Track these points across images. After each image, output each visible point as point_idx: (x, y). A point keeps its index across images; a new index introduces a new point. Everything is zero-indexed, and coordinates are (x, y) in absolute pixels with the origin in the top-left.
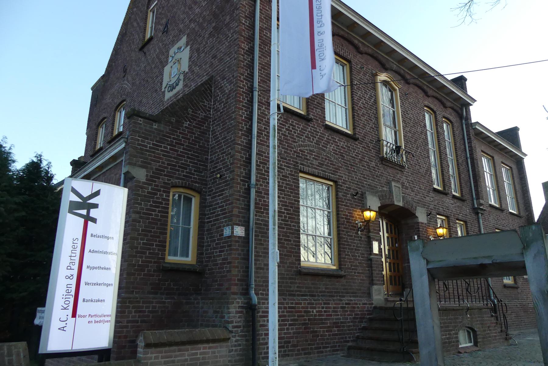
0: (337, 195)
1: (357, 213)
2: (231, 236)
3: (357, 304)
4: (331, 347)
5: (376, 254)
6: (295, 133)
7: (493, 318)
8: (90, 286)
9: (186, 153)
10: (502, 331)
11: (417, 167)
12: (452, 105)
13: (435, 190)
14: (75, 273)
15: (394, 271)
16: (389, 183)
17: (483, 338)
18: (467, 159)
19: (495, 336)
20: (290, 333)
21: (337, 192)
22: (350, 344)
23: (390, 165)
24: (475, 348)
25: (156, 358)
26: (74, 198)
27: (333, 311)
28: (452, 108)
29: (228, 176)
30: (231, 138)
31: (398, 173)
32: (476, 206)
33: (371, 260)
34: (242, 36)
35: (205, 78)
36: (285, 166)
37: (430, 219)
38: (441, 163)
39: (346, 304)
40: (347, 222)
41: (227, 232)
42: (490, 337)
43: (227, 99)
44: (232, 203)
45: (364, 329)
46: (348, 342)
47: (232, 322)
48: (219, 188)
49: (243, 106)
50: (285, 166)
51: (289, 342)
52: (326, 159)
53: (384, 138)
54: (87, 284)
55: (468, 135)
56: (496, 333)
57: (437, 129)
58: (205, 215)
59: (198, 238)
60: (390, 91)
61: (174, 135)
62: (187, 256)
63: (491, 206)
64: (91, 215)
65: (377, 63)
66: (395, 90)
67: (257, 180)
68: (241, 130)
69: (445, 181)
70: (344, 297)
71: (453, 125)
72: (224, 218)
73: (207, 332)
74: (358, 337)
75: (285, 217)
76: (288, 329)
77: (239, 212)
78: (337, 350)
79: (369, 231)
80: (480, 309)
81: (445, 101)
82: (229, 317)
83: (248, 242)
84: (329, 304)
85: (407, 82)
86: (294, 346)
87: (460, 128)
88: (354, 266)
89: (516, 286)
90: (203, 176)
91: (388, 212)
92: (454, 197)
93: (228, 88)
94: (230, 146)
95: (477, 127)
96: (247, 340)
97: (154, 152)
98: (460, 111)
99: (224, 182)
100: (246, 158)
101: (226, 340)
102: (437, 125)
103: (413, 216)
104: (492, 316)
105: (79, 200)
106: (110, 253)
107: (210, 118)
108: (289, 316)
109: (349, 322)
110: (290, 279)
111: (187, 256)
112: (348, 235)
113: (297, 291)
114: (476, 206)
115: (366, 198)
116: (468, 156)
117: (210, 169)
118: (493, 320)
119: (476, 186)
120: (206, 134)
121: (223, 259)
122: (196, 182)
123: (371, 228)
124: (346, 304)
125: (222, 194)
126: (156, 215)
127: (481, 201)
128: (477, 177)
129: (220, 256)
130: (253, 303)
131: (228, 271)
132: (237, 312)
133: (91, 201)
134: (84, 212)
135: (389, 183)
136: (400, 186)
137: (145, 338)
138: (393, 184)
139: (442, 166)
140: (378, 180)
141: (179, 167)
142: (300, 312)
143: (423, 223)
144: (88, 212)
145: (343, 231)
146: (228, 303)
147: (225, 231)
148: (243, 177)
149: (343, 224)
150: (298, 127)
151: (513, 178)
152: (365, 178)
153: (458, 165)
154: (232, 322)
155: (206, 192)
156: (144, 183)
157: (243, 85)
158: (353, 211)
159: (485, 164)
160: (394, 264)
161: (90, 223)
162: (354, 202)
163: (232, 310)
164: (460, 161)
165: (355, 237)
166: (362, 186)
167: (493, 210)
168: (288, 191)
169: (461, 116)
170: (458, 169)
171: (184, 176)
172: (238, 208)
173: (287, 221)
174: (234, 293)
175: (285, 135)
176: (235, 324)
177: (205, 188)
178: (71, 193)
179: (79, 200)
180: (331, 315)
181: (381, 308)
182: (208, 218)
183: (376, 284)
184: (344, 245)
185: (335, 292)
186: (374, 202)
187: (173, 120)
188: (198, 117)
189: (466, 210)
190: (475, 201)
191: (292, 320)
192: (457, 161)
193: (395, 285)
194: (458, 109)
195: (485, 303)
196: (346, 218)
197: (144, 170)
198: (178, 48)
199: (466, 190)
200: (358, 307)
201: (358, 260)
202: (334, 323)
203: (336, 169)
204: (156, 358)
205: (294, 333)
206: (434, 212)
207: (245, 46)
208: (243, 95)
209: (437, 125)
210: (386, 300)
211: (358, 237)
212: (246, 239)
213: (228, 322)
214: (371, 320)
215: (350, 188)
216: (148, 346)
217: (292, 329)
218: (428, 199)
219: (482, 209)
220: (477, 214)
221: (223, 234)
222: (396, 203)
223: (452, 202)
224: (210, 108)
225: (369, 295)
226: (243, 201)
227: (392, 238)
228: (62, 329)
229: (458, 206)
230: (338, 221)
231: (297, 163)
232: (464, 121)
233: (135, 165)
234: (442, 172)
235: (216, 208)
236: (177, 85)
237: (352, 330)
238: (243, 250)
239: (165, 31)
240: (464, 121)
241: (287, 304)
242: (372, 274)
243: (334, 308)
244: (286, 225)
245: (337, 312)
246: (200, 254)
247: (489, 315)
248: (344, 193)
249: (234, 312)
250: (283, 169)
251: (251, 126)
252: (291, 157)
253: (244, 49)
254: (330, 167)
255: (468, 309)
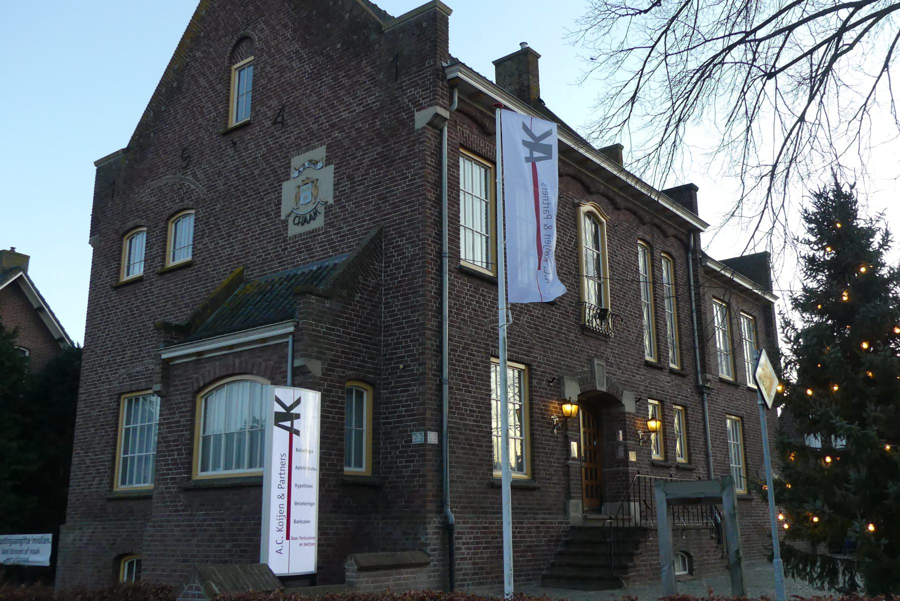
0: (530, 382)
1: (553, 405)
2: (425, 444)
3: (552, 523)
4: (525, 575)
5: (574, 459)
6: (485, 305)
7: (712, 541)
8: (299, 506)
9: (360, 336)
10: (722, 558)
11: (626, 333)
12: (675, 232)
13: (647, 364)
14: (285, 492)
15: (591, 478)
16: (590, 361)
17: (700, 565)
18: (692, 312)
19: (714, 564)
20: (483, 558)
21: (530, 378)
22: (544, 572)
23: (593, 335)
24: (690, 577)
25: (367, 582)
26: (278, 408)
27: (527, 532)
28: (675, 237)
29: (415, 367)
30: (418, 320)
31: (601, 345)
32: (701, 383)
33: (568, 466)
34: (428, 182)
35: (373, 233)
36: (476, 351)
37: (639, 406)
38: (656, 322)
39: (542, 523)
40: (543, 418)
41: (417, 438)
42: (708, 564)
43: (409, 266)
44: (424, 403)
45: (560, 554)
46: (542, 569)
47: (430, 544)
48: (401, 382)
49: (432, 278)
50: (476, 351)
51: (483, 568)
52: (519, 336)
53: (587, 300)
54: (296, 504)
55: (696, 276)
56: (715, 559)
57: (653, 272)
58: (380, 413)
59: (373, 444)
60: (594, 223)
61: (346, 313)
62: (361, 466)
63: (722, 380)
64: (295, 427)
65: (579, 186)
66: (601, 223)
67: (450, 374)
68: (431, 311)
69: (660, 352)
70: (537, 514)
71: (674, 262)
72: (412, 421)
73: (408, 556)
74: (553, 564)
75: (477, 416)
76: (482, 553)
77: (432, 415)
78: (531, 580)
79: (567, 429)
80: (698, 529)
81: (664, 226)
82: (427, 539)
83: (442, 451)
84: (522, 523)
85: (616, 207)
86: (487, 573)
87: (685, 266)
88: (549, 475)
89: (749, 497)
90: (377, 364)
91: (588, 401)
92: (672, 371)
93: (409, 252)
94: (417, 330)
95: (708, 264)
96: (443, 565)
97: (327, 339)
98: (685, 241)
99: (409, 376)
100: (437, 346)
101: (426, 564)
102: (653, 266)
103: (619, 403)
104: (712, 538)
105: (283, 411)
106: (305, 468)
107: (381, 285)
108: (483, 538)
109: (543, 546)
110: (482, 493)
111: (361, 466)
112: (543, 436)
113: (489, 508)
114: (701, 383)
115: (564, 385)
116: (694, 307)
117: (385, 355)
118: (714, 543)
119: (703, 353)
120: (378, 307)
121: (412, 471)
122: (370, 373)
123: (569, 424)
124: (542, 523)
125: (408, 391)
126: (333, 418)
127: (709, 376)
128: (705, 337)
129: (409, 467)
130: (450, 522)
131: (420, 486)
132: (434, 533)
133: (294, 411)
134: (288, 424)
135: (589, 360)
136: (604, 364)
137: (356, 561)
138: (596, 361)
139: (657, 328)
140: (578, 357)
141: (353, 354)
142: (494, 533)
143: (630, 414)
144: (292, 424)
145: (537, 430)
146: (425, 523)
147: (414, 437)
148: (435, 370)
149: (538, 421)
150: (489, 297)
151: (757, 334)
152: (562, 356)
153: (679, 322)
154: (430, 544)
155: (380, 384)
156: (321, 379)
157: (431, 249)
158: (549, 402)
159: (717, 315)
160: (591, 469)
161: (294, 436)
162: (550, 390)
163: (430, 531)
164: (682, 317)
165: (550, 437)
166: (559, 368)
167: (725, 387)
168: (479, 384)
169: (686, 247)
170: (679, 328)
171: (358, 365)
172: (431, 409)
173: (478, 422)
174: (430, 512)
175: (475, 310)
176: (433, 547)
177: (379, 379)
178: (276, 403)
179: (283, 411)
180: (525, 537)
181: (579, 528)
182: (384, 419)
183: (573, 498)
184: (538, 448)
185: (529, 509)
186: (572, 389)
187: (345, 293)
188: (369, 286)
189: (687, 388)
190: (700, 375)
191: (486, 542)
192: (678, 316)
193: (592, 497)
194: (683, 237)
195: (705, 521)
196: (541, 414)
197: (319, 362)
198: (310, 161)
199: (688, 361)
200: (553, 528)
201: (553, 466)
202: (529, 546)
203: (530, 348)
204: (367, 582)
205: (488, 558)
206: (644, 396)
207: (431, 196)
208: (431, 264)
209: (654, 265)
210: (585, 518)
211: (554, 437)
212: (439, 447)
213: (426, 545)
214: (567, 543)
215: (545, 372)
216: (361, 569)
217: (486, 553)
218: (638, 377)
219: (708, 388)
220: (701, 394)
221: (411, 441)
222: (599, 388)
223: (668, 379)
224: (381, 271)
225: (565, 511)
226: (435, 400)
227: (589, 434)
228: (279, 552)
229: (677, 385)
230: (531, 417)
231: (488, 345)
232: (690, 255)
233: (310, 356)
234: (658, 335)
235: (399, 407)
236: (313, 218)
237: (547, 555)
238: (436, 461)
239: (279, 121)
240: (690, 255)
241: (481, 523)
242: (569, 484)
243: (528, 528)
244: (478, 426)
245: (531, 533)
246: (375, 463)
247: (708, 537)
248: (539, 379)
249: (431, 534)
250: (474, 355)
251: (441, 303)
252: (482, 339)
253: (430, 200)
254: (523, 346)
255: (684, 529)
